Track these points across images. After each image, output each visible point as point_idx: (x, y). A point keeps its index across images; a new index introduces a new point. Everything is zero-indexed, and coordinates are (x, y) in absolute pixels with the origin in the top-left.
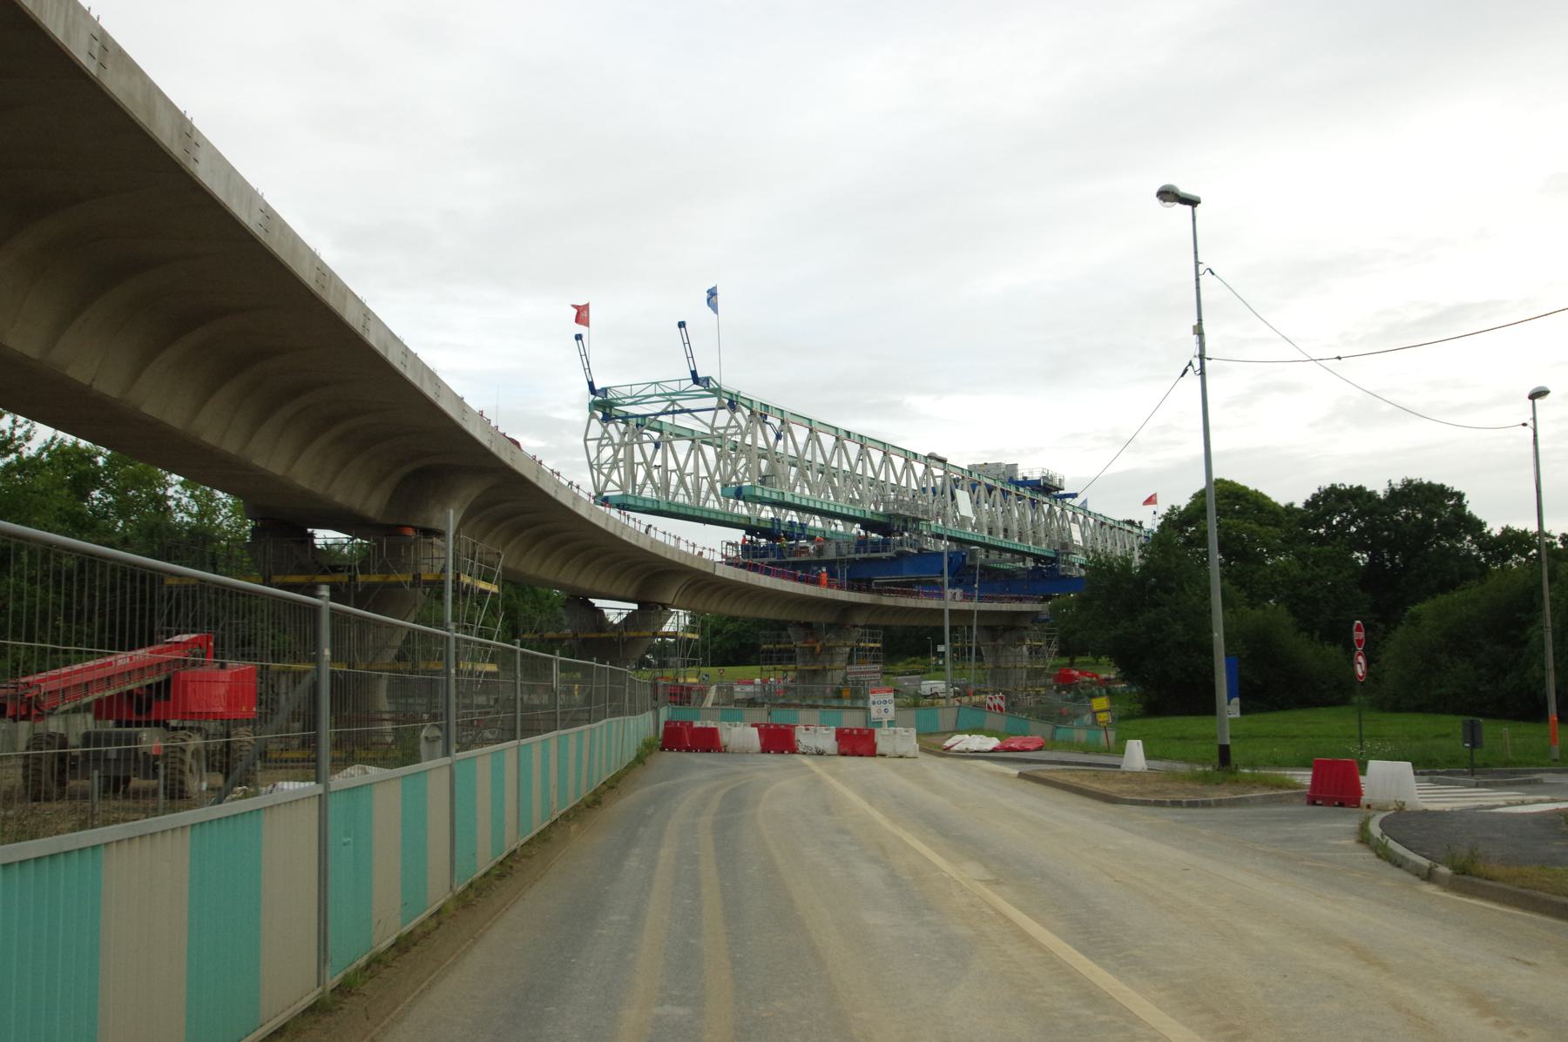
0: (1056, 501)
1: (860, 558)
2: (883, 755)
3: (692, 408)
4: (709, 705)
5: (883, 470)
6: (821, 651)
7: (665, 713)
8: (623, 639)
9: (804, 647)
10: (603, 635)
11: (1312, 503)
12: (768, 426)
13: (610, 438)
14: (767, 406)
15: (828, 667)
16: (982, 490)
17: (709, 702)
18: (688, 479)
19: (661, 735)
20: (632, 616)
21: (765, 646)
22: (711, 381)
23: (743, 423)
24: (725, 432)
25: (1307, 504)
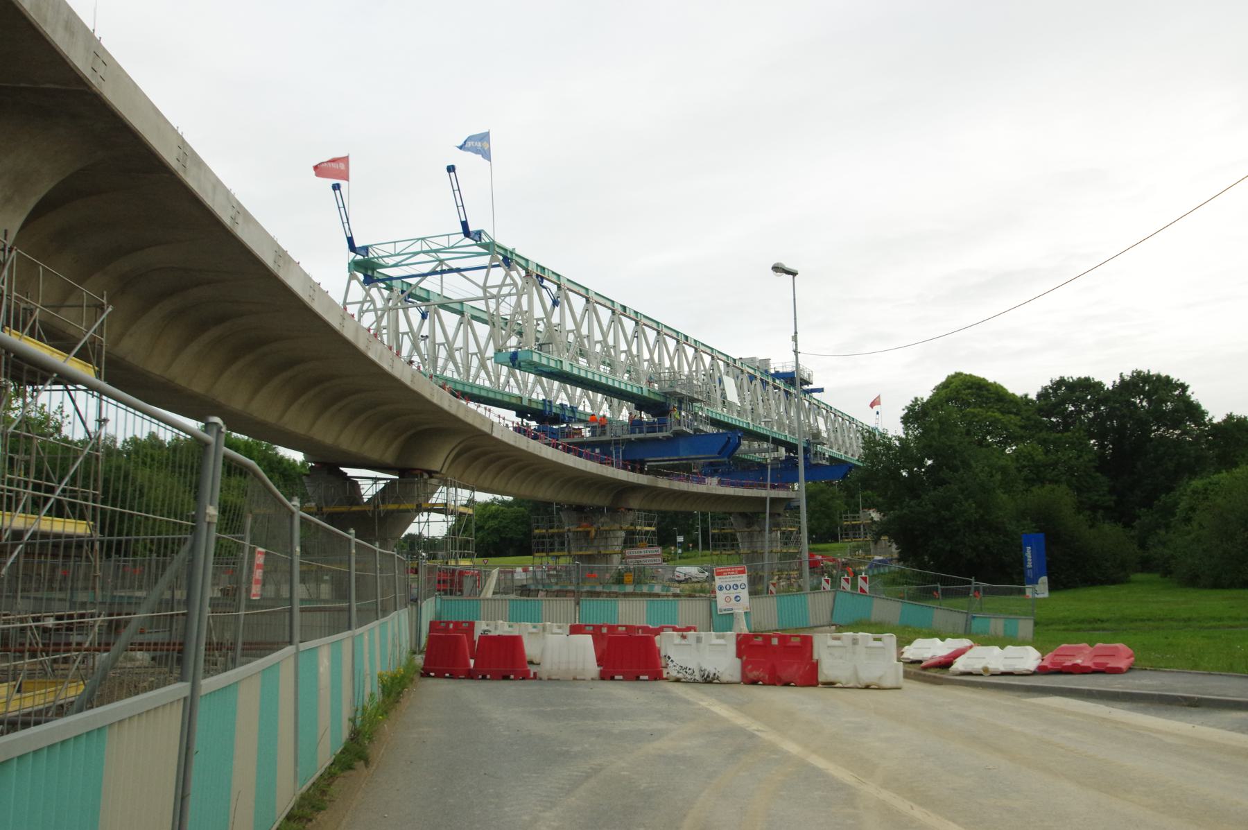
0: (805, 395)
1: (635, 439)
2: (830, 684)
3: (462, 267)
4: (490, 595)
6: (596, 535)
7: (429, 609)
8: (379, 513)
9: (577, 532)
10: (355, 508)
11: (1043, 395)
12: (544, 290)
13: (373, 301)
14: (544, 269)
15: (603, 552)
16: (745, 377)
17: (488, 592)
18: (457, 354)
19: (424, 640)
20: (390, 486)
21: (537, 531)
22: (483, 236)
23: (520, 283)
24: (499, 292)
25: (1039, 396)
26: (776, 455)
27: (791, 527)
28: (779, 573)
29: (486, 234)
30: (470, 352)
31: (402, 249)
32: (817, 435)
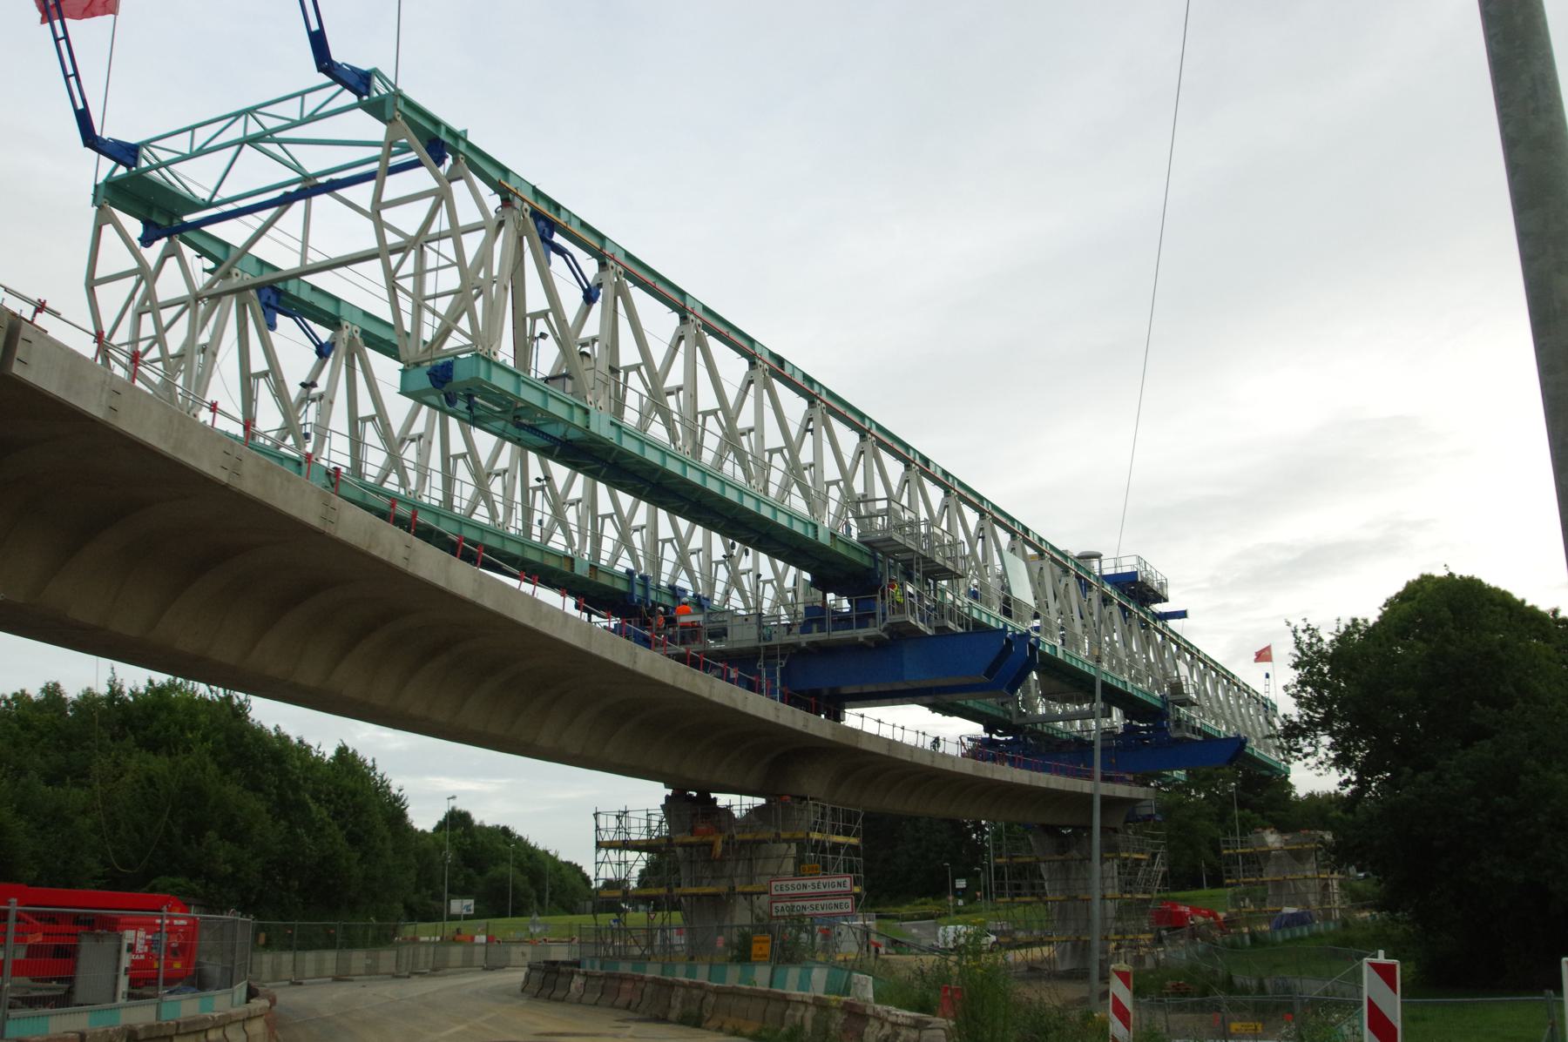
5: (860, 468)
6: (725, 851)
22: (376, 82)
26: (1105, 723)
27: (1137, 852)
28: (1118, 937)
29: (382, 77)
30: (452, 453)
31: (206, 139)
32: (1177, 687)
